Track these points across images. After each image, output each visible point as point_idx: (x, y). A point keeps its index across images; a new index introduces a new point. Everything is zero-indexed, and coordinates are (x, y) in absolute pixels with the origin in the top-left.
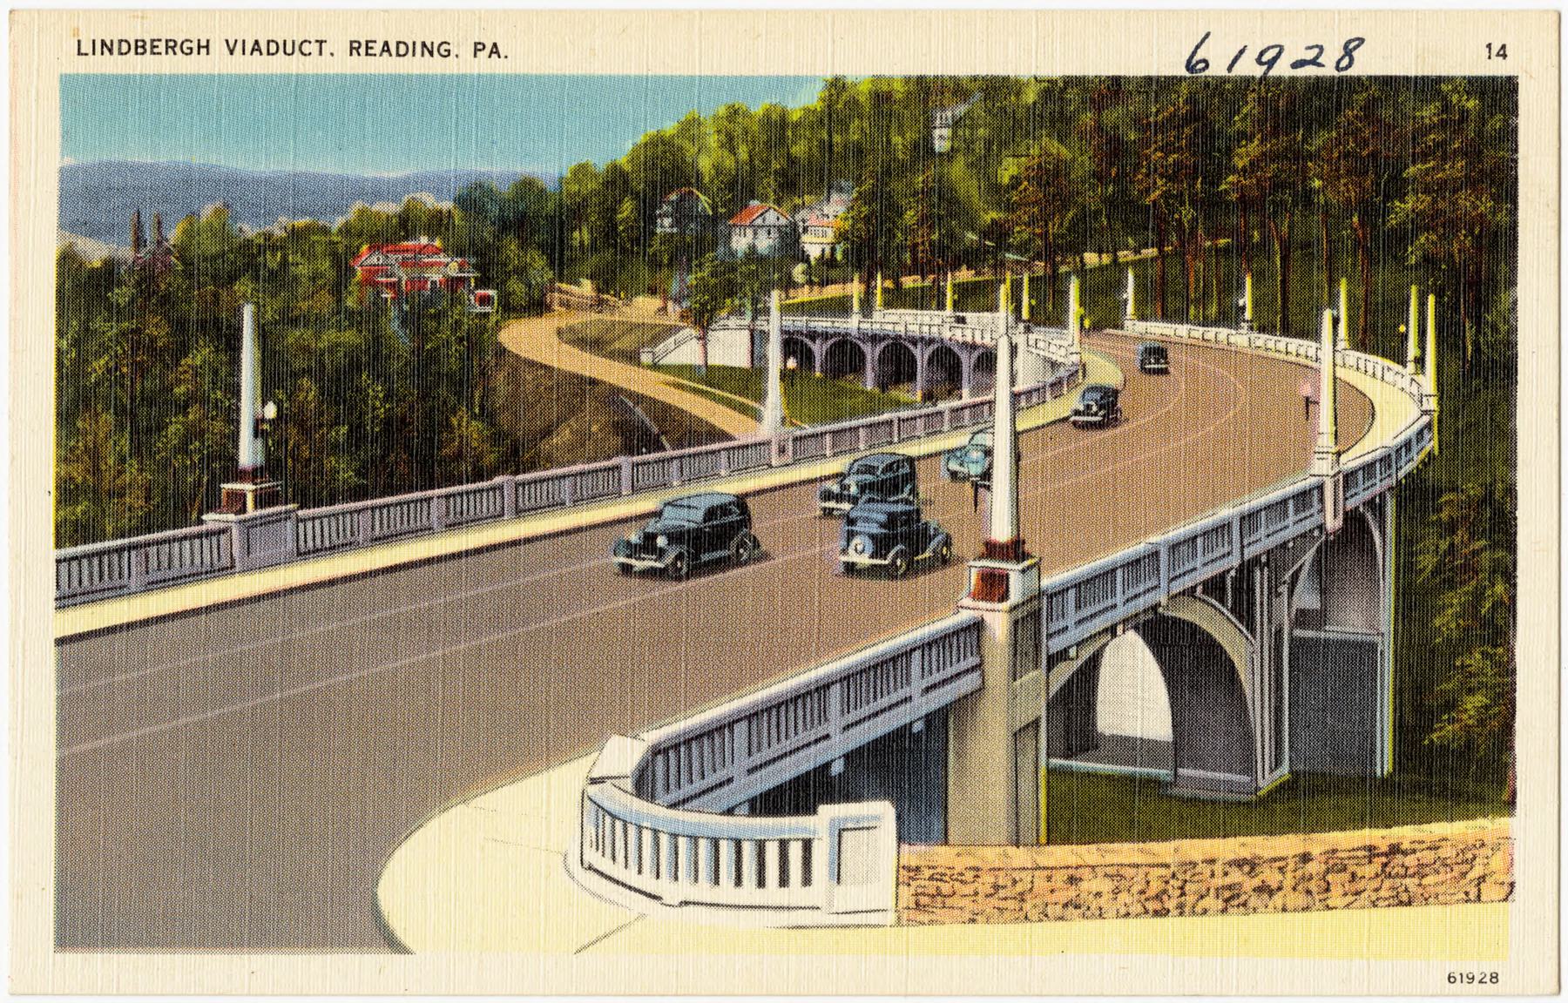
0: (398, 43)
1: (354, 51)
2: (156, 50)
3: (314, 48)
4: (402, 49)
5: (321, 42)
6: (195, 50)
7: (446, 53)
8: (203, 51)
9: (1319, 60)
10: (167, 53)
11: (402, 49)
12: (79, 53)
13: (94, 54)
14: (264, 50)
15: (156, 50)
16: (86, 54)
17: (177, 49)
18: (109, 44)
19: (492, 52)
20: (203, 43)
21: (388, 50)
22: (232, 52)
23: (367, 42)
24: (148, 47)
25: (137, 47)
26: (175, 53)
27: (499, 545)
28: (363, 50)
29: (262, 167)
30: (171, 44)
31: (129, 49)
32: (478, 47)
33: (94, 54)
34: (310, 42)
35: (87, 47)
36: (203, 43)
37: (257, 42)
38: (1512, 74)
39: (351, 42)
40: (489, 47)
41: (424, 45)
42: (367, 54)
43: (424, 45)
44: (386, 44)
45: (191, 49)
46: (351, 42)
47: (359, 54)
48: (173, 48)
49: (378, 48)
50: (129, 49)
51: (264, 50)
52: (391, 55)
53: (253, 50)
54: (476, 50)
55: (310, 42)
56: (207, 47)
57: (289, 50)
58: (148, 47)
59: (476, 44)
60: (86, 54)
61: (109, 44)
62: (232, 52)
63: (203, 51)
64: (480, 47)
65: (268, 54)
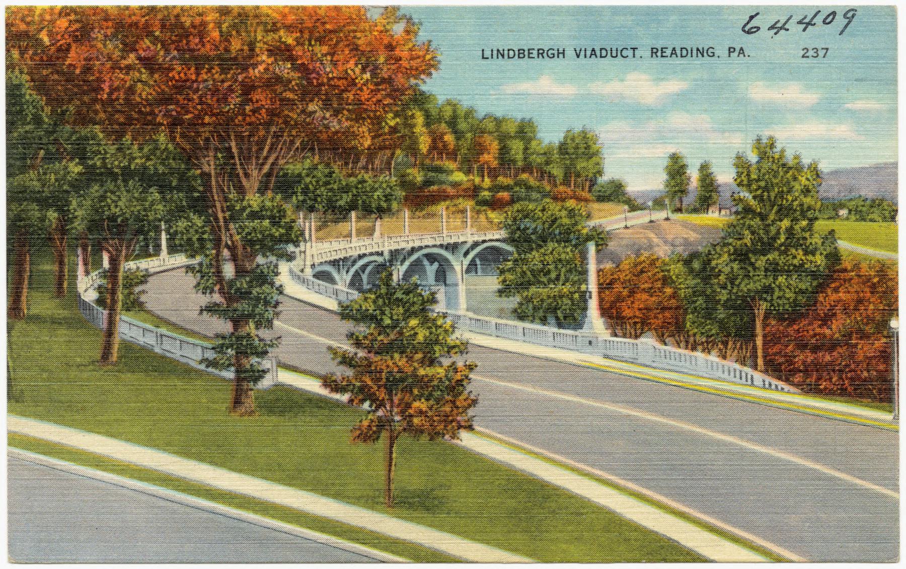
0: (601, 50)
1: (540, 56)
2: (531, 56)
3: (630, 53)
4: (684, 52)
5: (634, 49)
6: (556, 56)
7: (712, 54)
8: (561, 56)
9: (787, 26)
10: (538, 57)
11: (684, 52)
12: (483, 58)
13: (492, 57)
14: (679, 55)
15: (531, 56)
16: (487, 58)
17: (545, 55)
18: (499, 55)
19: (739, 53)
20: (561, 51)
21: (676, 54)
22: (578, 56)
23: (529, 50)
24: (526, 53)
25: (519, 54)
26: (543, 57)
27: (312, 376)
28: (659, 54)
29: (867, 328)
30: (541, 52)
31: (514, 55)
32: (731, 50)
33: (492, 57)
34: (627, 49)
35: (488, 53)
36: (561, 51)
37: (593, 50)
38: (528, 116)
39: (652, 49)
40: (738, 50)
41: (698, 50)
42: (529, 57)
43: (698, 50)
44: (674, 49)
45: (554, 54)
46: (652, 49)
47: (657, 56)
48: (656, 53)
49: (668, 52)
50: (514, 55)
51: (679, 55)
52: (596, 57)
53: (591, 55)
54: (730, 52)
55: (627, 49)
56: (563, 53)
57: (614, 54)
58: (526, 53)
59: (730, 48)
60: (487, 58)
61: (500, 56)
62: (578, 56)
63: (561, 56)
64: (732, 50)
65: (509, 57)
